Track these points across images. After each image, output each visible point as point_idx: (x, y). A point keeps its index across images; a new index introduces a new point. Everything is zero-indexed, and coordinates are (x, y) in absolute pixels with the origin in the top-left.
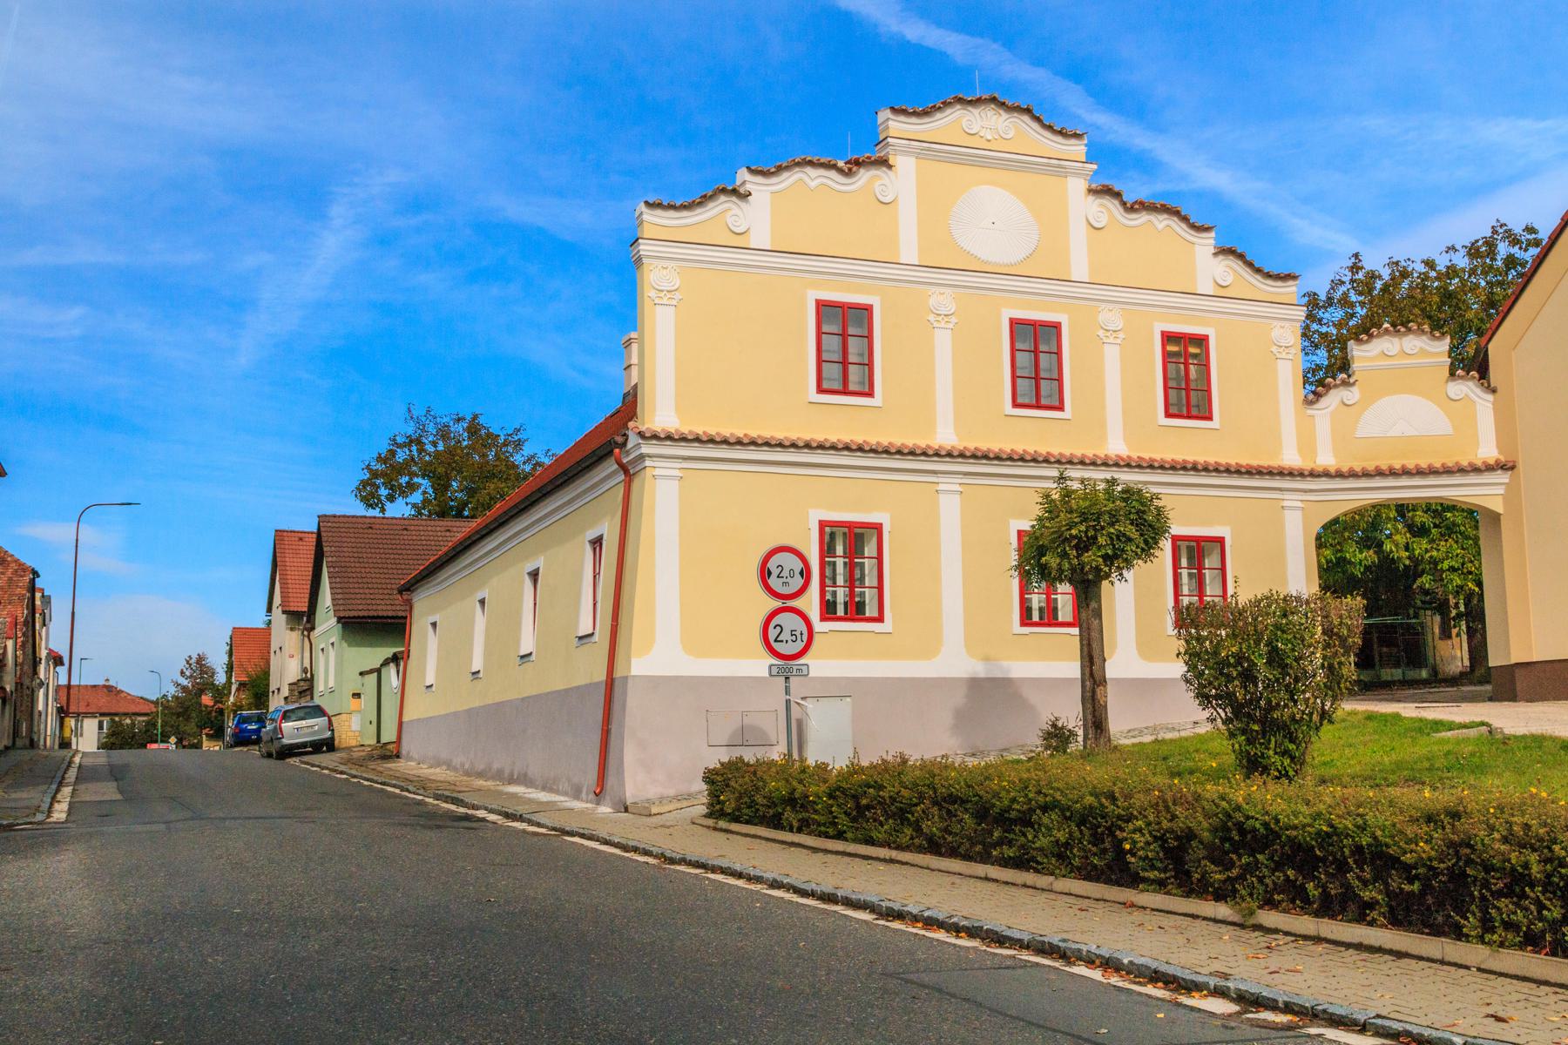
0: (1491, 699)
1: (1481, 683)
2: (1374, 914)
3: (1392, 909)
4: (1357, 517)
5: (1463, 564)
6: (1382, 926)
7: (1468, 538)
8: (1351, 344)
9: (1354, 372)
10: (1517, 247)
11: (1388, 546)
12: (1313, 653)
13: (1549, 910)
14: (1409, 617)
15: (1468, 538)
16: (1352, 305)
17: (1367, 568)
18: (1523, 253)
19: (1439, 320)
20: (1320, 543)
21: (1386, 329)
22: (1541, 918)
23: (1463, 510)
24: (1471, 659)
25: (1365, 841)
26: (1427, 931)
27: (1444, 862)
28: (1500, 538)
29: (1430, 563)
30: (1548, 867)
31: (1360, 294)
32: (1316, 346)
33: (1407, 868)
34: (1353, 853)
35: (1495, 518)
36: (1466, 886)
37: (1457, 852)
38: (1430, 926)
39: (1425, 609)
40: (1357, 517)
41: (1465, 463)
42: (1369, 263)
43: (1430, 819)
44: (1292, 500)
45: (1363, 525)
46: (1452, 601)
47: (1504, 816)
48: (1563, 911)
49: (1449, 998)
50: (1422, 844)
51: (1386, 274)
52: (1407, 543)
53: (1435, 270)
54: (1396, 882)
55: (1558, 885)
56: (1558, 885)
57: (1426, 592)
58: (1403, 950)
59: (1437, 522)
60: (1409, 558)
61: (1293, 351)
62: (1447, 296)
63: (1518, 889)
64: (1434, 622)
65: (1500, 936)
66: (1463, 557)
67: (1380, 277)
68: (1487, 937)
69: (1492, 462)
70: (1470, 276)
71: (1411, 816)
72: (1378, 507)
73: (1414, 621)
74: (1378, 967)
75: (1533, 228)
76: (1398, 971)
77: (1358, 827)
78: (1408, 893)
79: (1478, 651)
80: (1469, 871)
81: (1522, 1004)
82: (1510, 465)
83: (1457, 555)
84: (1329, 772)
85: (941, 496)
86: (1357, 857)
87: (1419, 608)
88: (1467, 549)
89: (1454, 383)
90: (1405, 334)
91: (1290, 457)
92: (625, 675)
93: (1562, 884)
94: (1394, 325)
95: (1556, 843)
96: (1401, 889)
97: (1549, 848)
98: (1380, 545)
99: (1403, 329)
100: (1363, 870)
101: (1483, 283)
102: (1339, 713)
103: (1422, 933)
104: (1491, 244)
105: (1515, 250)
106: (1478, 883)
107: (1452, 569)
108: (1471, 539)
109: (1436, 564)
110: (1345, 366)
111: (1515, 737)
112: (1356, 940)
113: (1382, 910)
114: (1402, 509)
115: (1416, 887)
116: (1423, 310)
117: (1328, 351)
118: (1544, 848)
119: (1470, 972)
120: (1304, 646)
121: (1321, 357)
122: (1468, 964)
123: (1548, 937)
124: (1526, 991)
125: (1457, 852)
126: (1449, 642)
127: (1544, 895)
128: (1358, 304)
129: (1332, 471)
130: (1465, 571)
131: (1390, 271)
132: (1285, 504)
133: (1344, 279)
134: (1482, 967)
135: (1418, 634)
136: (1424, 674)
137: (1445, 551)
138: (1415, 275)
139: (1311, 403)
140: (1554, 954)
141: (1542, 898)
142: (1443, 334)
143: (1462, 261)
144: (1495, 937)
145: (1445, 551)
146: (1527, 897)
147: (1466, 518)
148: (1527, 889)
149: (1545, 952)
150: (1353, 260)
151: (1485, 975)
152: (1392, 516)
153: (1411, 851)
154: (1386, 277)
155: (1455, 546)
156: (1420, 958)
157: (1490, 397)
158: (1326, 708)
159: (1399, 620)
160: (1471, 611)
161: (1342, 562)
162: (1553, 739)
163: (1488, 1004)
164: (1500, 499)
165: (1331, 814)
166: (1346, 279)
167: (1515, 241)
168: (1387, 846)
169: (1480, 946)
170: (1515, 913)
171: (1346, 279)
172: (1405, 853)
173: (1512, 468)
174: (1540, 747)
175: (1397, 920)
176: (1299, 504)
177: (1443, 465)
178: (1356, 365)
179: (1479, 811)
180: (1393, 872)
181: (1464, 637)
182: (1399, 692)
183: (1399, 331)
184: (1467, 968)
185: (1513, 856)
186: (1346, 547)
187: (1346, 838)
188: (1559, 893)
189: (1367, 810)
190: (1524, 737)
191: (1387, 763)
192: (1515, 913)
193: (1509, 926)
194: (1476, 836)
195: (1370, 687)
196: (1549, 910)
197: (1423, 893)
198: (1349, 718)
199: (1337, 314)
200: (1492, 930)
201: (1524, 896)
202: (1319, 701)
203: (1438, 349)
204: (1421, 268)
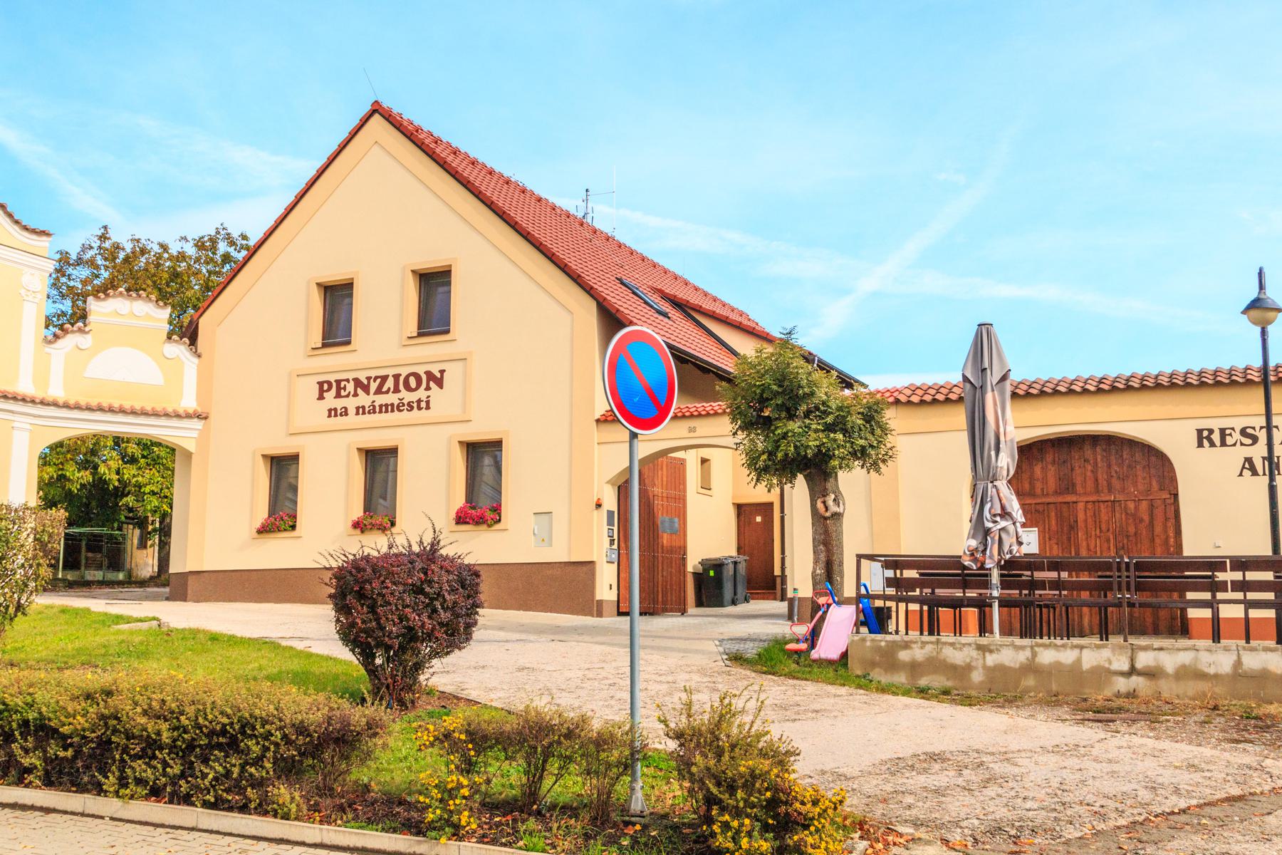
0: (167, 599)
1: (164, 585)
2: (31, 778)
3: (47, 773)
4: (79, 442)
5: (161, 489)
6: (37, 787)
7: (168, 469)
8: (90, 299)
9: (89, 323)
10: (234, 247)
11: (102, 469)
12: (15, 554)
13: (172, 767)
14: (113, 529)
15: (168, 469)
16: (98, 267)
17: (83, 486)
18: (237, 253)
19: (166, 292)
20: (44, 461)
21: (121, 293)
22: (165, 774)
23: (167, 447)
24: (159, 566)
25: (31, 716)
26: (74, 789)
27: (95, 732)
28: (190, 471)
29: (135, 486)
30: (175, 733)
31: (106, 259)
32: (63, 296)
33: (64, 737)
34: (19, 726)
35: (188, 455)
36: (110, 750)
37: (106, 724)
38: (77, 785)
39: (128, 524)
40: (79, 442)
41: (170, 410)
42: (116, 236)
43: (89, 697)
44: (22, 423)
45: (83, 450)
46: (151, 519)
47: (147, 693)
48: (182, 768)
49: (81, 845)
50: (79, 718)
51: (128, 247)
52: (119, 468)
53: (167, 252)
54: (54, 749)
55: (181, 747)
56: (181, 747)
57: (131, 510)
58: (52, 806)
59: (145, 454)
60: (119, 480)
61: (39, 296)
62: (175, 275)
63: (150, 752)
64: (134, 535)
65: (131, 790)
66: (162, 484)
67: (123, 249)
68: (122, 791)
69: (191, 411)
70: (195, 263)
71: (72, 694)
72: (98, 438)
73: (117, 532)
74: (27, 822)
75: (246, 236)
76: (43, 825)
77: (27, 704)
78: (62, 758)
79: (164, 562)
80: (114, 739)
81: (141, 844)
82: (204, 415)
83: (158, 482)
84: (16, 657)
85: (15, 432)
86: (23, 730)
87: (123, 523)
88: (166, 478)
89: (170, 345)
90: (135, 299)
91: (25, 387)
92: (189, 597)
93: (184, 746)
94: (128, 290)
95: (183, 715)
96: (57, 756)
97: (178, 719)
98: (96, 467)
99: (134, 295)
100: (26, 740)
101: (204, 271)
102: (33, 606)
103: (70, 791)
104: (213, 241)
105: (231, 250)
106: (120, 748)
107: (153, 493)
108: (170, 470)
109: (140, 487)
110: (83, 316)
111: (177, 630)
112: (11, 801)
113: (38, 774)
114: (118, 441)
115: (70, 753)
116: (154, 282)
117: (73, 302)
118: (174, 718)
119: (104, 821)
120: (8, 548)
121: (67, 306)
122: (103, 815)
123: (168, 789)
124: (145, 833)
125: (106, 724)
126: (145, 551)
127: (169, 756)
128: (102, 267)
129: (61, 402)
130: (162, 495)
131: (132, 246)
132: (15, 425)
133: (93, 245)
134: (114, 816)
135: (120, 543)
136: (121, 576)
137: (147, 477)
138: (152, 254)
139: (50, 342)
140: (171, 802)
141: (167, 758)
142: (166, 304)
143: (190, 250)
144: (128, 791)
145: (147, 477)
146: (157, 758)
147: (169, 453)
148: (157, 752)
149: (164, 801)
150: (102, 230)
151: (116, 823)
152: (109, 445)
153: (70, 724)
154: (129, 250)
155: (157, 474)
156: (65, 812)
157: (196, 360)
158: (22, 602)
159: (105, 530)
160: (164, 528)
161: (62, 478)
162: (205, 632)
163: (113, 847)
164: (193, 442)
165: (4, 693)
166: (95, 245)
167: (232, 243)
168: (50, 720)
169: (115, 799)
170: (145, 771)
171: (95, 245)
172: (64, 725)
173: (206, 418)
174: (193, 639)
175: (49, 782)
176: (28, 426)
177: (153, 409)
178: (91, 318)
179: (128, 690)
180: (52, 741)
181: (157, 548)
182: (98, 590)
183: (131, 296)
184: (102, 818)
185: (149, 726)
186: (67, 467)
187: (15, 713)
188: (181, 754)
189: (37, 689)
190: (184, 630)
191: (70, 650)
192: (145, 771)
193: (140, 782)
194: (123, 710)
195: (54, 586)
196: (172, 767)
197: (75, 757)
198: (46, 611)
199: (84, 272)
200: (126, 786)
201: (154, 757)
202: (16, 596)
203: (163, 315)
204: (156, 249)
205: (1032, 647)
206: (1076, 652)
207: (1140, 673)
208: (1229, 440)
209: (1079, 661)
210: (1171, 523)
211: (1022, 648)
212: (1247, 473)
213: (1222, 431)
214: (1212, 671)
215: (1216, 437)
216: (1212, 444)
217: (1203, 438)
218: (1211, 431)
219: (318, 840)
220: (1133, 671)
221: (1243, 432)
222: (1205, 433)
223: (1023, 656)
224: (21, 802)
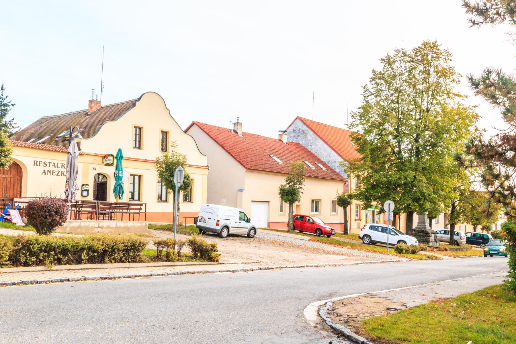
205: (80, 222)
206: (89, 223)
207: (100, 228)
208: (41, 165)
209: (89, 225)
210: (19, 185)
211: (78, 222)
212: (44, 174)
213: (40, 162)
214: (112, 226)
215: (38, 163)
216: (37, 165)
217: (35, 163)
218: (37, 162)
219: (154, 266)
220: (99, 227)
221: (44, 163)
222: (36, 162)
223: (78, 224)
224: (83, 268)
